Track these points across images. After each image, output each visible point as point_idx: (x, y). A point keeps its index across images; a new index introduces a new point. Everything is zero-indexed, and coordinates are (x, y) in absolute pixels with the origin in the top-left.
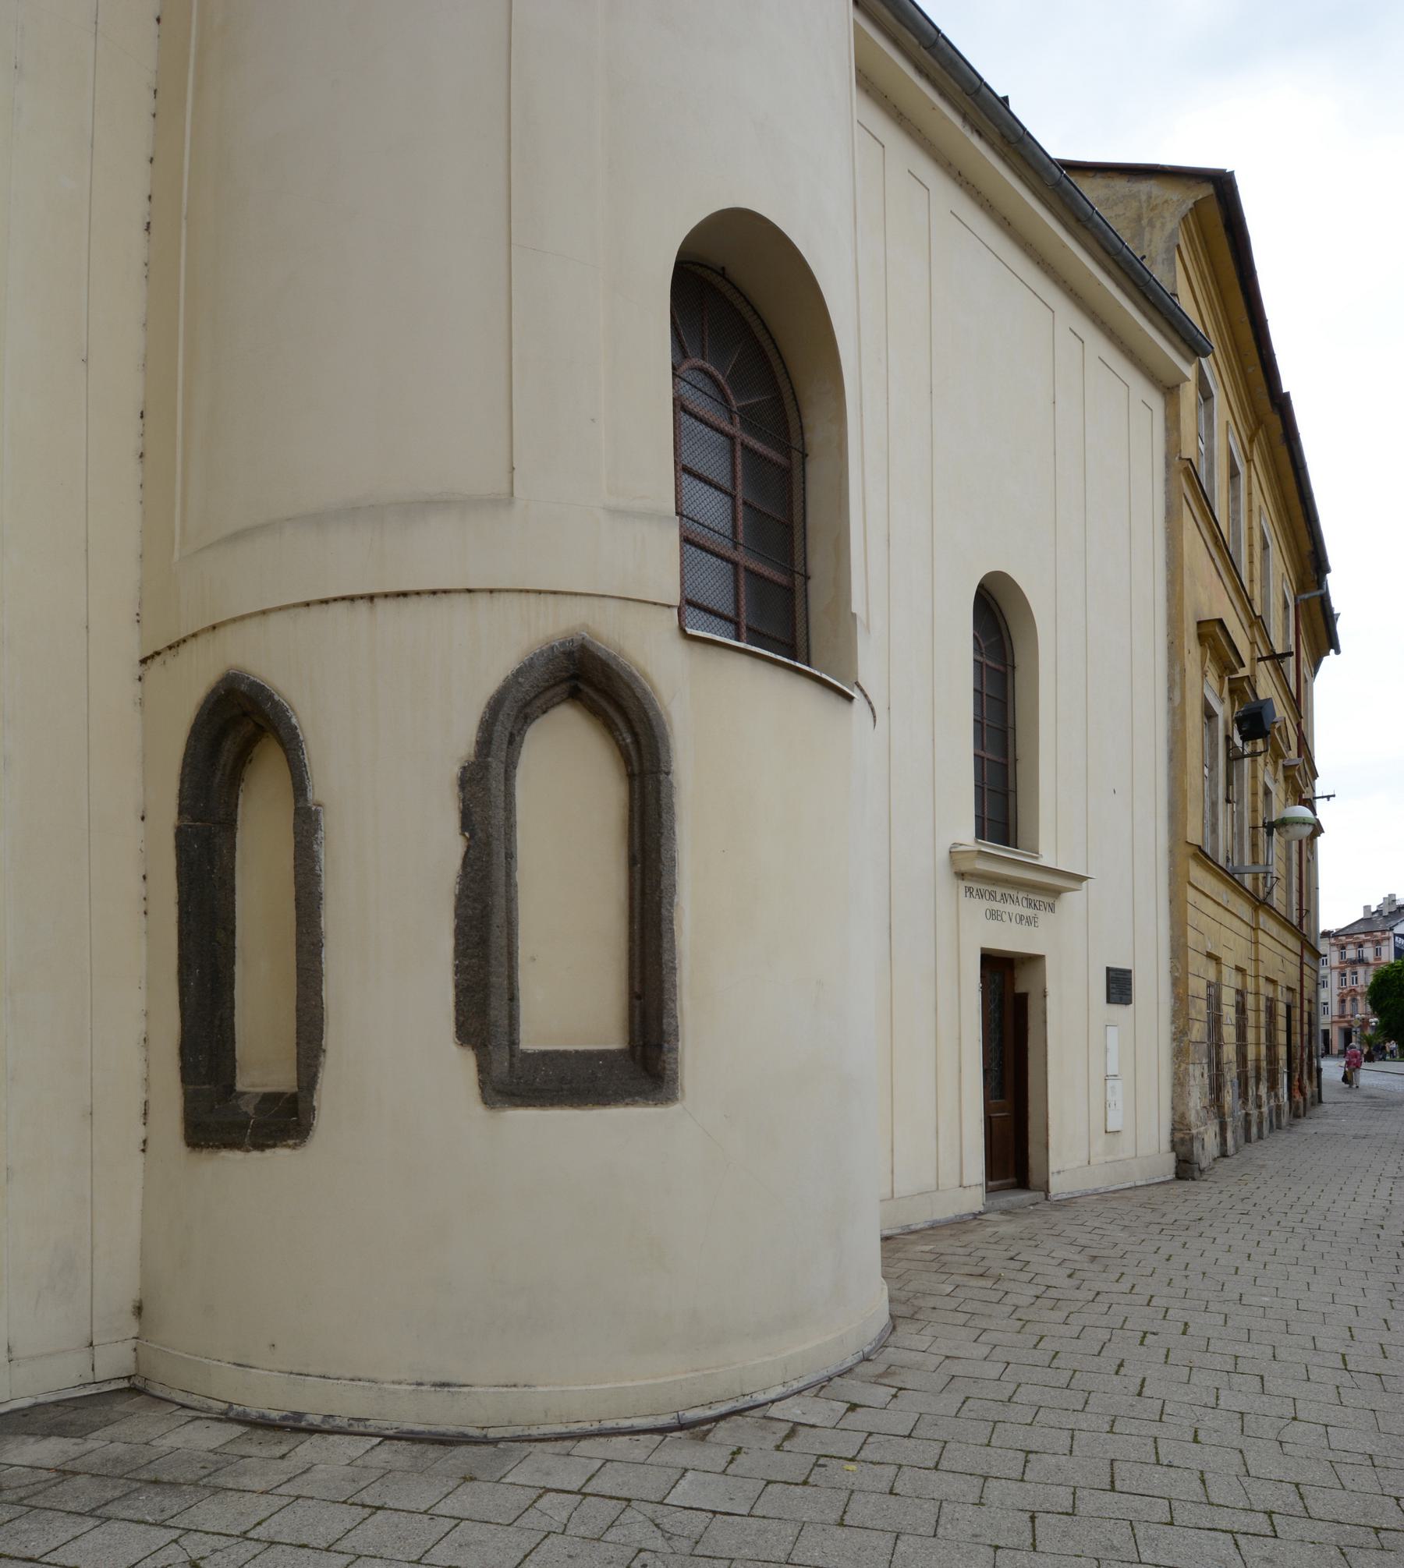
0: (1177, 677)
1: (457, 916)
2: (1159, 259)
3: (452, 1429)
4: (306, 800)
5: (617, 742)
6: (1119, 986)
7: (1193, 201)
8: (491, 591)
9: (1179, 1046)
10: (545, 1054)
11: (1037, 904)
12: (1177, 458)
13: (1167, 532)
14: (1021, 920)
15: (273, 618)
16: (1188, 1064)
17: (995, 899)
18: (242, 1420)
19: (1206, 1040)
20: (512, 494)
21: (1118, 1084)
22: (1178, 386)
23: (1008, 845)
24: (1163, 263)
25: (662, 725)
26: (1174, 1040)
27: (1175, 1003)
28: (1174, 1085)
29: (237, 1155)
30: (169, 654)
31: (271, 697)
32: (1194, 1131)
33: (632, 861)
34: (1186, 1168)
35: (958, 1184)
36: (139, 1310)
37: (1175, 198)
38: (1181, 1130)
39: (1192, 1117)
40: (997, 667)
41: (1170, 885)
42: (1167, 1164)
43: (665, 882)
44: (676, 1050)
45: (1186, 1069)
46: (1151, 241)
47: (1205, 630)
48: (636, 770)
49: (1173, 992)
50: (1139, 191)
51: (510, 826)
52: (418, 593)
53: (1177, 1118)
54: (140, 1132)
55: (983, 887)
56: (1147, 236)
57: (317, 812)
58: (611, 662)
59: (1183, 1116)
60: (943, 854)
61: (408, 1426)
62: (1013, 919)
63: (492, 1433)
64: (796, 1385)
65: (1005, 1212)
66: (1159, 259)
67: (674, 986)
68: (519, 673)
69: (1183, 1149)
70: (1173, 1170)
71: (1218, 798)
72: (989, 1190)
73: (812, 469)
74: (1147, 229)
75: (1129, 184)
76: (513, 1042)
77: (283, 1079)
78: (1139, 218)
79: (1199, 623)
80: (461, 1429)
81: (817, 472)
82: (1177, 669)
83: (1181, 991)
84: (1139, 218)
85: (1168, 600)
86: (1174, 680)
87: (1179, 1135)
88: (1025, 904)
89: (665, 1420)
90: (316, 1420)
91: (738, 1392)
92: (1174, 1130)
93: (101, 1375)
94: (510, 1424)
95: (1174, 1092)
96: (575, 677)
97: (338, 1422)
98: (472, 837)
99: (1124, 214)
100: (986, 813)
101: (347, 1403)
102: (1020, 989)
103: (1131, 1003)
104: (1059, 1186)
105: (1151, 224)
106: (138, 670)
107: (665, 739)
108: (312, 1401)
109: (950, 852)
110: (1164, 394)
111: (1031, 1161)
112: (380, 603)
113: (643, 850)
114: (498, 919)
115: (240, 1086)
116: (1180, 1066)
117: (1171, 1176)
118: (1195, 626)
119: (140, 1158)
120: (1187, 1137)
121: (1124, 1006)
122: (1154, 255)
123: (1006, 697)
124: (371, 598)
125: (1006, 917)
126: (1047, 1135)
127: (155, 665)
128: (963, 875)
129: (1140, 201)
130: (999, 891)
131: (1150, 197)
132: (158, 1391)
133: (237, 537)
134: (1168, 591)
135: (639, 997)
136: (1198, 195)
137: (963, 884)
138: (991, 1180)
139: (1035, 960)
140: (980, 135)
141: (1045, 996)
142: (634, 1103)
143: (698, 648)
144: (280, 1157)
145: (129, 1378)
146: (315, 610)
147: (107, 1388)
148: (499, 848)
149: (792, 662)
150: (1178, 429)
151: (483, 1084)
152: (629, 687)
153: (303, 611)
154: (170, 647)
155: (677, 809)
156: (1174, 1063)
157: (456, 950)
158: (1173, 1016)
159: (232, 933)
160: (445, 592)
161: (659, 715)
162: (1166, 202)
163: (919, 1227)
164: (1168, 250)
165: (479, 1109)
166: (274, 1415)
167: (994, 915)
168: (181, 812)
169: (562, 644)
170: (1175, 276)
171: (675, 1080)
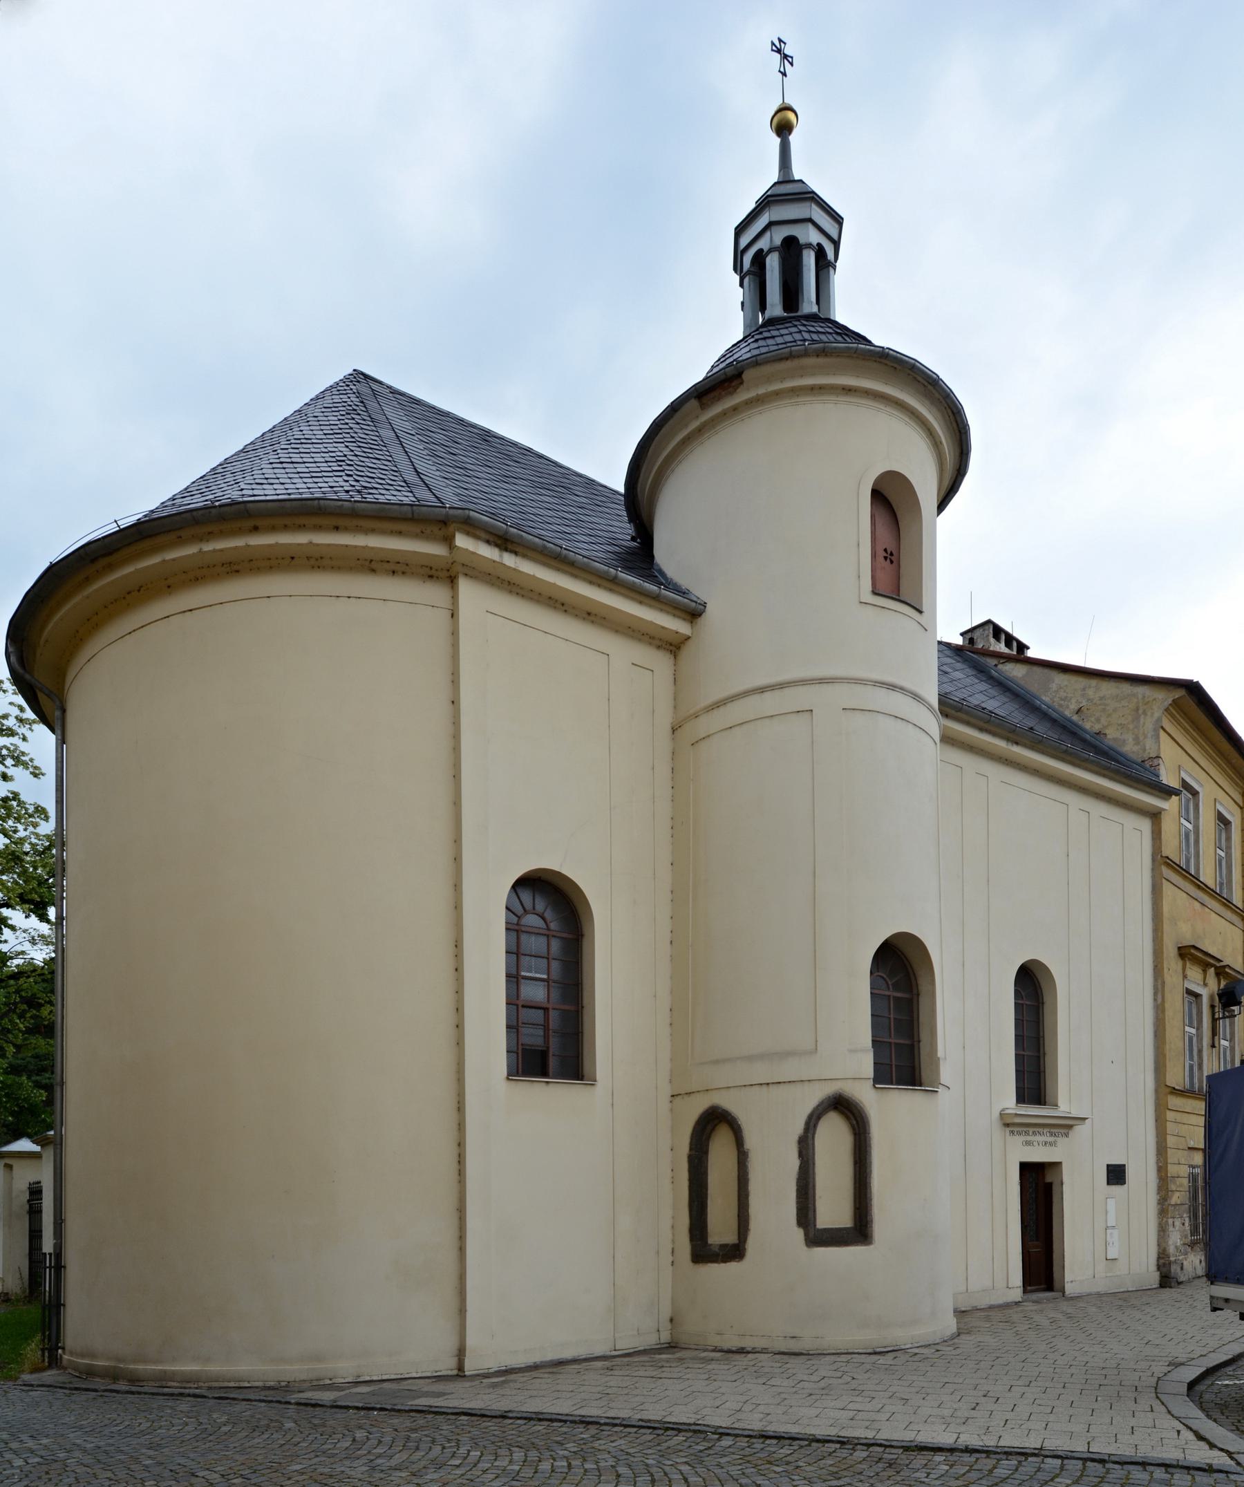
0: (1160, 987)
1: (797, 1185)
2: (1149, 735)
3: (797, 1351)
4: (744, 1148)
5: (850, 1123)
6: (1116, 1175)
7: (1172, 699)
8: (809, 1081)
9: (1162, 1208)
10: (825, 1229)
11: (1057, 1134)
12: (1159, 856)
13: (1152, 901)
14: (1045, 1144)
15: (732, 1089)
16: (1168, 1218)
17: (1029, 1134)
18: (721, 1351)
19: (1187, 1202)
20: (816, 1049)
21: (1115, 1232)
22: (1160, 813)
23: (1040, 1105)
24: (1152, 738)
25: (867, 1118)
26: (1158, 1204)
27: (1160, 1181)
28: (1159, 1231)
29: (716, 1265)
30: (686, 1097)
31: (730, 1114)
32: (1172, 1259)
33: (855, 1163)
34: (1167, 1280)
35: (1005, 1286)
36: (671, 1320)
37: (1160, 698)
38: (1163, 1258)
39: (1171, 1250)
40: (1033, 1004)
41: (1156, 1111)
42: (1154, 1278)
43: (868, 1171)
44: (872, 1227)
45: (1167, 1222)
46: (1144, 723)
47: (1183, 952)
48: (857, 1132)
49: (1158, 1174)
50: (1137, 692)
51: (814, 1154)
52: (784, 1082)
53: (1161, 1251)
54: (671, 1259)
55: (1020, 1129)
56: (1142, 720)
57: (747, 1152)
58: (850, 1100)
59: (1164, 1250)
60: (996, 1114)
61: (782, 1350)
62: (1041, 1144)
63: (811, 1352)
64: (916, 1345)
65: (1034, 1302)
66: (1149, 735)
67: (871, 1205)
68: (819, 1106)
69: (1164, 1270)
70: (1158, 1282)
71: (1202, 1047)
72: (1025, 1292)
73: (921, 999)
74: (1143, 716)
75: (1132, 688)
76: (815, 1226)
77: (731, 1238)
78: (1137, 709)
79: (1179, 948)
80: (800, 1351)
81: (923, 1002)
82: (1160, 982)
83: (1163, 1174)
84: (1137, 709)
85: (1154, 940)
86: (1158, 989)
87: (1162, 1261)
88: (1048, 1134)
89: (870, 1351)
90: (750, 1349)
91: (895, 1344)
92: (1159, 1258)
93: (662, 1341)
94: (817, 1349)
95: (1159, 1235)
96: (837, 1103)
97: (757, 1350)
98: (802, 1159)
99: (1128, 706)
100: (1026, 1084)
101: (760, 1343)
102: (1048, 1180)
103: (1125, 1183)
104: (1070, 1289)
105: (1145, 713)
106: (670, 1099)
107: (868, 1122)
108: (748, 1343)
109: (1000, 1114)
110: (1151, 818)
111: (1054, 1275)
112: (771, 1085)
113: (860, 1158)
114: (811, 1186)
115: (710, 1241)
116: (1162, 1220)
117: (1157, 1285)
118: (1176, 950)
119: (671, 1268)
120: (1167, 1262)
121: (1120, 1186)
122: (1146, 732)
123: (1039, 1019)
124: (768, 1084)
125: (1035, 1144)
126: (1064, 1261)
127: (678, 1099)
128: (1008, 1124)
129: (1138, 698)
130: (1031, 1130)
131: (1144, 697)
132: (683, 1346)
133: (716, 1062)
134: (1153, 935)
135: (858, 1209)
136: (1174, 696)
137: (1008, 1130)
138: (1030, 1286)
139: (1057, 1165)
140: (1017, 743)
141: (1062, 1184)
142: (857, 1245)
143: (879, 1090)
144: (733, 1266)
145: (669, 1343)
146: (747, 1088)
147: (663, 1346)
148: (811, 1162)
149: (914, 1088)
150: (1160, 839)
151: (806, 1240)
152: (855, 1106)
153: (744, 1088)
154: (686, 1094)
155: (872, 1146)
156: (1159, 1218)
157: (797, 1197)
158: (1158, 1190)
159: (707, 1190)
160: (794, 1082)
161: (866, 1115)
162: (1155, 699)
163: (982, 1307)
164: (1155, 730)
165: (805, 1248)
166: (734, 1349)
167: (1028, 1143)
168: (691, 1149)
169: (833, 1095)
170: (1159, 746)
171: (871, 1237)
